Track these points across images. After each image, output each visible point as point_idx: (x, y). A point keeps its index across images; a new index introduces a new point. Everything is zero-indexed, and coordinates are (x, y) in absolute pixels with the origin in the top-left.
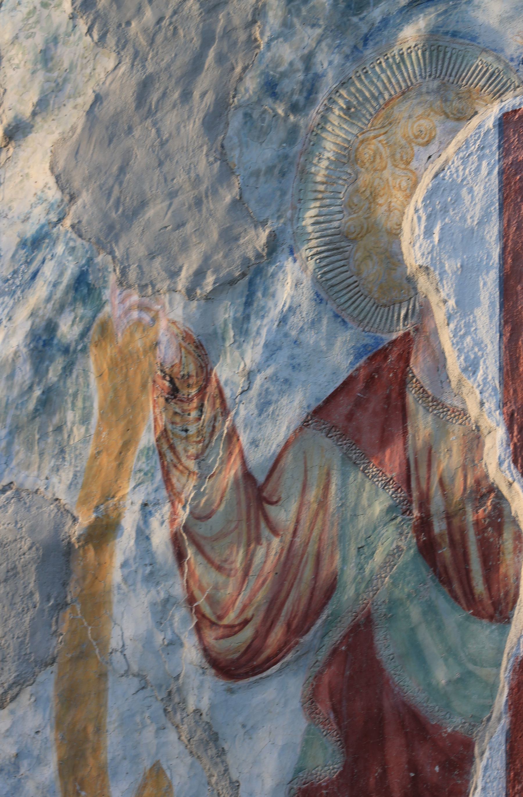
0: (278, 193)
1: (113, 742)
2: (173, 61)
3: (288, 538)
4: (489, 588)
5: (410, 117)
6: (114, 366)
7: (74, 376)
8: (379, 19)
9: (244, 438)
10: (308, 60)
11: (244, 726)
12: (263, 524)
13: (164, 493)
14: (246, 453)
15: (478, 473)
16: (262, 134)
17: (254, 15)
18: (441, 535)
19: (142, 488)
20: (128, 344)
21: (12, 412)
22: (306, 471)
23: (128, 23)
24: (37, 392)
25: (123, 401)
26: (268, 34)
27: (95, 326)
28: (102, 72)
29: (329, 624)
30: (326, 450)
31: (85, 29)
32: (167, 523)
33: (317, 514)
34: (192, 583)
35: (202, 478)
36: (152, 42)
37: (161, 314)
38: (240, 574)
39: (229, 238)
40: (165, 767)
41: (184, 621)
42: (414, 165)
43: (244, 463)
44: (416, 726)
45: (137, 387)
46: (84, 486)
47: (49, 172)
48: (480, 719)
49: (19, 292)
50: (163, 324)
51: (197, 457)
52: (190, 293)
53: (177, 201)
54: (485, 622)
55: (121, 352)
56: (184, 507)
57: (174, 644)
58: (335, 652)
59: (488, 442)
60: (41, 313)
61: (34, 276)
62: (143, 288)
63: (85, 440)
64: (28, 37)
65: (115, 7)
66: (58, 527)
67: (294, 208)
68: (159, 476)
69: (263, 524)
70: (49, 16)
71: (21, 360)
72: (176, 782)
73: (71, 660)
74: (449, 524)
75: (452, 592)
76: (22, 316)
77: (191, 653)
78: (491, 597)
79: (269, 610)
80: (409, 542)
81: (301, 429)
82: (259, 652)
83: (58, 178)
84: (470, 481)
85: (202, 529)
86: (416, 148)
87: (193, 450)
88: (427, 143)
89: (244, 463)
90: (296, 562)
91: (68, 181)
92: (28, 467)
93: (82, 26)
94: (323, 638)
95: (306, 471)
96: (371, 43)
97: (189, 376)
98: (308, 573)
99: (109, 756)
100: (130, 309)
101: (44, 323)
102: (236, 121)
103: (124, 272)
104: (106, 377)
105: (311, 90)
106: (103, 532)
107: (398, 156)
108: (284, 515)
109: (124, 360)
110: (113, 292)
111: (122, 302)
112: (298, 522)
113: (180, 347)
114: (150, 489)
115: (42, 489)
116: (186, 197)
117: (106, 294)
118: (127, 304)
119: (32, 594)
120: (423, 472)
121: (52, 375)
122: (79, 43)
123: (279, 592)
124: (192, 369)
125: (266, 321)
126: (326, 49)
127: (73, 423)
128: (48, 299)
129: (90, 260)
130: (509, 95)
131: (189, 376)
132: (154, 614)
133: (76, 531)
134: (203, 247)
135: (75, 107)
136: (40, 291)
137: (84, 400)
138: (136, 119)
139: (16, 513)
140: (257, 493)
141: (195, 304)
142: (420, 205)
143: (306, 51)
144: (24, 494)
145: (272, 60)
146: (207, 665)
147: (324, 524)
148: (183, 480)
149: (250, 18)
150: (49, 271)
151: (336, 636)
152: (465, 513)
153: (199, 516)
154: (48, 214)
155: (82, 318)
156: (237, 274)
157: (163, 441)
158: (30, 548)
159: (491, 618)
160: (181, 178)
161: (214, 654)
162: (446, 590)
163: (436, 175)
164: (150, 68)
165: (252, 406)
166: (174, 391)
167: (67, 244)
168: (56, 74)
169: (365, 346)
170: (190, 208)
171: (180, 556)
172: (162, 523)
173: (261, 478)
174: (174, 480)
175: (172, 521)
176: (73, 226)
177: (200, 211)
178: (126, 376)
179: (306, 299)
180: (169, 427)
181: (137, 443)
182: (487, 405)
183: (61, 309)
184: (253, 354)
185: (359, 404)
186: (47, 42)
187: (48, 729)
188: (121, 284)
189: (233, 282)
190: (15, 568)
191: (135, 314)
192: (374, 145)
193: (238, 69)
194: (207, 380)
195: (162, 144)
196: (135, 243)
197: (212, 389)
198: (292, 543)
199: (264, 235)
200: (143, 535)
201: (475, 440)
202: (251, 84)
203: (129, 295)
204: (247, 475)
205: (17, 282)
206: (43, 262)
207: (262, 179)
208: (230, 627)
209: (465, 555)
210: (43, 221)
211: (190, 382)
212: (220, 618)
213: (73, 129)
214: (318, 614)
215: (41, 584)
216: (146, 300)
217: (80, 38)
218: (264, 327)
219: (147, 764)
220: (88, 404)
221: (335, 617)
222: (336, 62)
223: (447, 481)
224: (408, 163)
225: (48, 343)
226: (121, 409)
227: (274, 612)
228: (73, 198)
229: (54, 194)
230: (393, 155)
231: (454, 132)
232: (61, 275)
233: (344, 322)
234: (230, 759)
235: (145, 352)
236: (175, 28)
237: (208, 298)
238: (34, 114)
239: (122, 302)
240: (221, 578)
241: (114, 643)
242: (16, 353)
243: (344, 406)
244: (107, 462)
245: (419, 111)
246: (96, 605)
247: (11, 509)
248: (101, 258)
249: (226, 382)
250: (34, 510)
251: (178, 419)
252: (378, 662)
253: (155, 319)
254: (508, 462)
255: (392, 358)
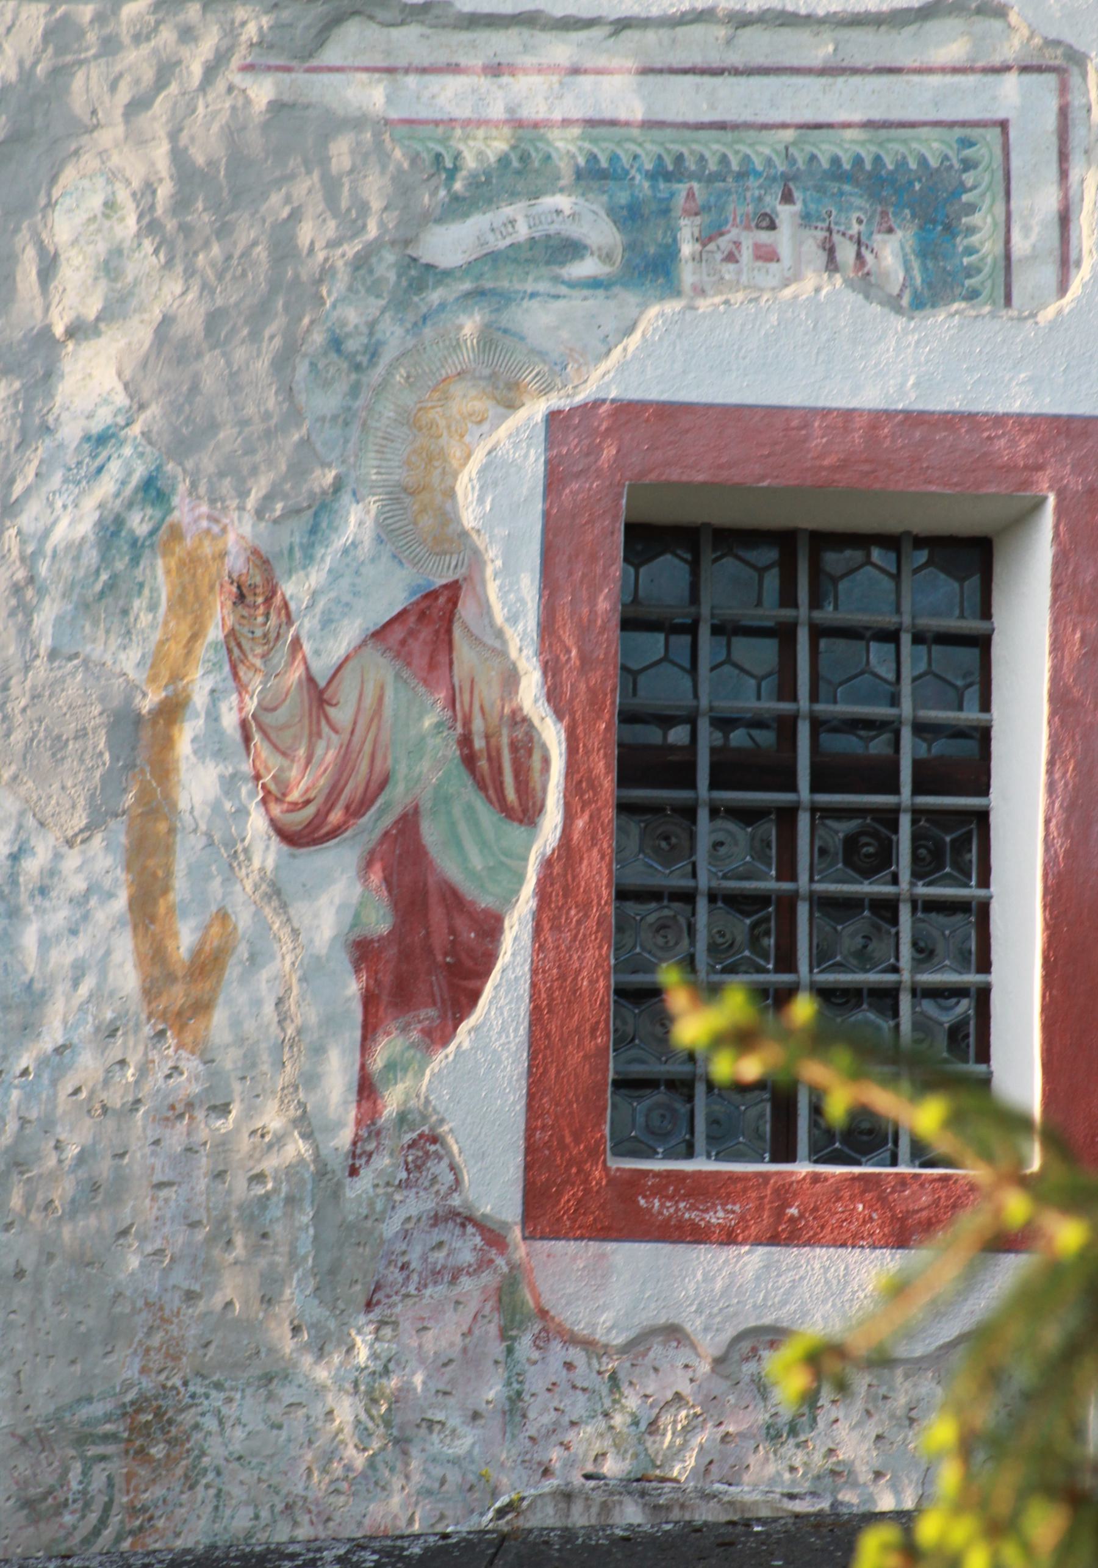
0: (341, 441)
1: (181, 887)
2: (242, 299)
3: (346, 736)
4: (520, 798)
5: (465, 396)
6: (182, 564)
7: (141, 567)
8: (436, 303)
9: (307, 647)
10: (372, 325)
11: (304, 885)
12: (323, 722)
13: (231, 683)
14: (309, 661)
15: (514, 704)
16: (327, 384)
17: (321, 273)
18: (481, 751)
19: (211, 676)
20: (196, 549)
21: (77, 590)
22: (362, 682)
23: (196, 254)
24: (104, 577)
25: (190, 597)
26: (335, 295)
27: (164, 528)
28: (171, 295)
29: (382, 812)
30: (380, 669)
31: (151, 250)
32: (235, 709)
33: (372, 720)
34: (258, 763)
35: (267, 677)
36: (220, 277)
37: (229, 528)
38: (303, 762)
39: (298, 470)
40: (230, 911)
41: (252, 795)
42: (467, 439)
43: (307, 669)
44: (454, 900)
45: (204, 590)
46: (152, 666)
47: (116, 378)
48: (510, 897)
49: (84, 483)
50: (231, 537)
51: (263, 656)
52: (259, 514)
53: (247, 430)
54: (516, 824)
55: (189, 554)
56: (251, 697)
57: (242, 812)
58: (386, 834)
59: (524, 683)
60: (109, 506)
61: (100, 470)
62: (212, 502)
63: (153, 626)
64: (89, 243)
65: (182, 235)
66: (128, 699)
67: (356, 456)
68: (227, 668)
69: (323, 722)
70: (111, 228)
71: (88, 545)
72: (241, 926)
73: (141, 815)
74: (488, 743)
75: (488, 797)
76: (89, 504)
77: (257, 822)
78: (521, 805)
79: (330, 794)
80: (454, 751)
81: (360, 647)
82: (318, 827)
83: (126, 386)
84: (507, 710)
85: (268, 719)
86: (470, 425)
87: (259, 650)
88: (480, 422)
89: (307, 669)
90: (354, 756)
91: (136, 391)
92: (94, 641)
93: (148, 246)
94: (374, 824)
95: (362, 682)
96: (429, 323)
97: (256, 586)
98: (363, 767)
99: (178, 899)
100: (200, 517)
101: (112, 517)
102: (302, 369)
103: (194, 485)
104: (174, 573)
105: (374, 352)
106: (172, 710)
107: (453, 429)
108: (341, 715)
109: (191, 561)
110: (182, 499)
111: (192, 510)
112: (355, 723)
113: (248, 559)
114: (218, 678)
115: (109, 663)
116: (258, 427)
117: (175, 501)
118: (197, 512)
119: (101, 754)
120: (466, 697)
121: (120, 565)
122: (145, 259)
123: (338, 781)
124: (258, 580)
125: (329, 550)
126: (388, 320)
127: (140, 609)
128: (117, 495)
129: (159, 468)
130: (554, 395)
131: (256, 586)
132: (222, 784)
133: (147, 703)
134: (272, 475)
135: (142, 322)
136: (106, 486)
137: (152, 590)
138: (205, 346)
139: (84, 680)
140: (319, 695)
141: (262, 525)
142: (474, 475)
143: (370, 318)
144: (91, 665)
145: (338, 319)
146: (272, 833)
147: (379, 728)
148: (250, 674)
149: (317, 276)
150: (115, 468)
151: (388, 821)
152: (500, 735)
153: (264, 708)
154: (115, 416)
155: (150, 518)
156: (305, 504)
157: (231, 639)
158: (101, 714)
159: (521, 822)
160: (250, 410)
161: (279, 825)
162: (482, 795)
163: (489, 453)
164: (219, 302)
165: (316, 621)
166: (241, 597)
167: (136, 448)
168: (119, 285)
169: (419, 586)
170: (259, 438)
171: (247, 739)
172: (231, 709)
173: (322, 683)
174: (241, 674)
175: (241, 710)
176: (143, 434)
177: (270, 443)
178: (194, 575)
179: (367, 538)
180: (237, 627)
181: (205, 636)
182: (525, 652)
183: (130, 505)
184: (316, 577)
185: (412, 633)
186: (110, 253)
187: (119, 870)
188: (190, 494)
189: (298, 511)
190: (85, 729)
191: (204, 524)
192: (432, 414)
193: (306, 321)
194: (274, 593)
195: (232, 375)
196: (207, 462)
197: (277, 601)
198: (350, 741)
199: (330, 476)
200: (213, 716)
201: (511, 679)
202: (318, 338)
203: (199, 506)
204: (311, 680)
205: (82, 473)
206: (109, 458)
207: (327, 425)
208: (295, 804)
209: (500, 771)
210: (109, 421)
211: (256, 592)
212: (284, 795)
213: (141, 343)
214: (372, 801)
215: (110, 745)
216: (216, 514)
217: (145, 257)
218: (329, 556)
219: (214, 909)
220: (155, 595)
221: (388, 805)
222: (397, 334)
223: (487, 709)
224: (462, 436)
225: (115, 534)
226: (188, 603)
227: (334, 796)
228: (142, 407)
229: (121, 399)
230: (449, 427)
231: (505, 418)
232: (130, 474)
233: (400, 562)
234: (292, 911)
235: (214, 559)
236: (244, 271)
237: (276, 522)
238: (98, 319)
239: (192, 510)
240: (286, 763)
241: (183, 804)
242: (83, 538)
243: (399, 632)
244: (176, 649)
245: (473, 393)
246: (163, 769)
247: (79, 677)
248: (170, 467)
249: (291, 597)
250: (103, 682)
251: (245, 622)
252: (424, 847)
253: (224, 530)
254: (543, 700)
255: (442, 600)
